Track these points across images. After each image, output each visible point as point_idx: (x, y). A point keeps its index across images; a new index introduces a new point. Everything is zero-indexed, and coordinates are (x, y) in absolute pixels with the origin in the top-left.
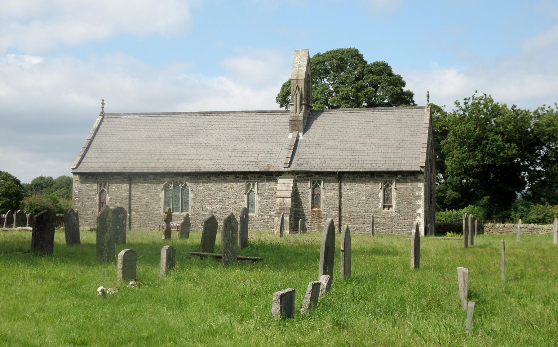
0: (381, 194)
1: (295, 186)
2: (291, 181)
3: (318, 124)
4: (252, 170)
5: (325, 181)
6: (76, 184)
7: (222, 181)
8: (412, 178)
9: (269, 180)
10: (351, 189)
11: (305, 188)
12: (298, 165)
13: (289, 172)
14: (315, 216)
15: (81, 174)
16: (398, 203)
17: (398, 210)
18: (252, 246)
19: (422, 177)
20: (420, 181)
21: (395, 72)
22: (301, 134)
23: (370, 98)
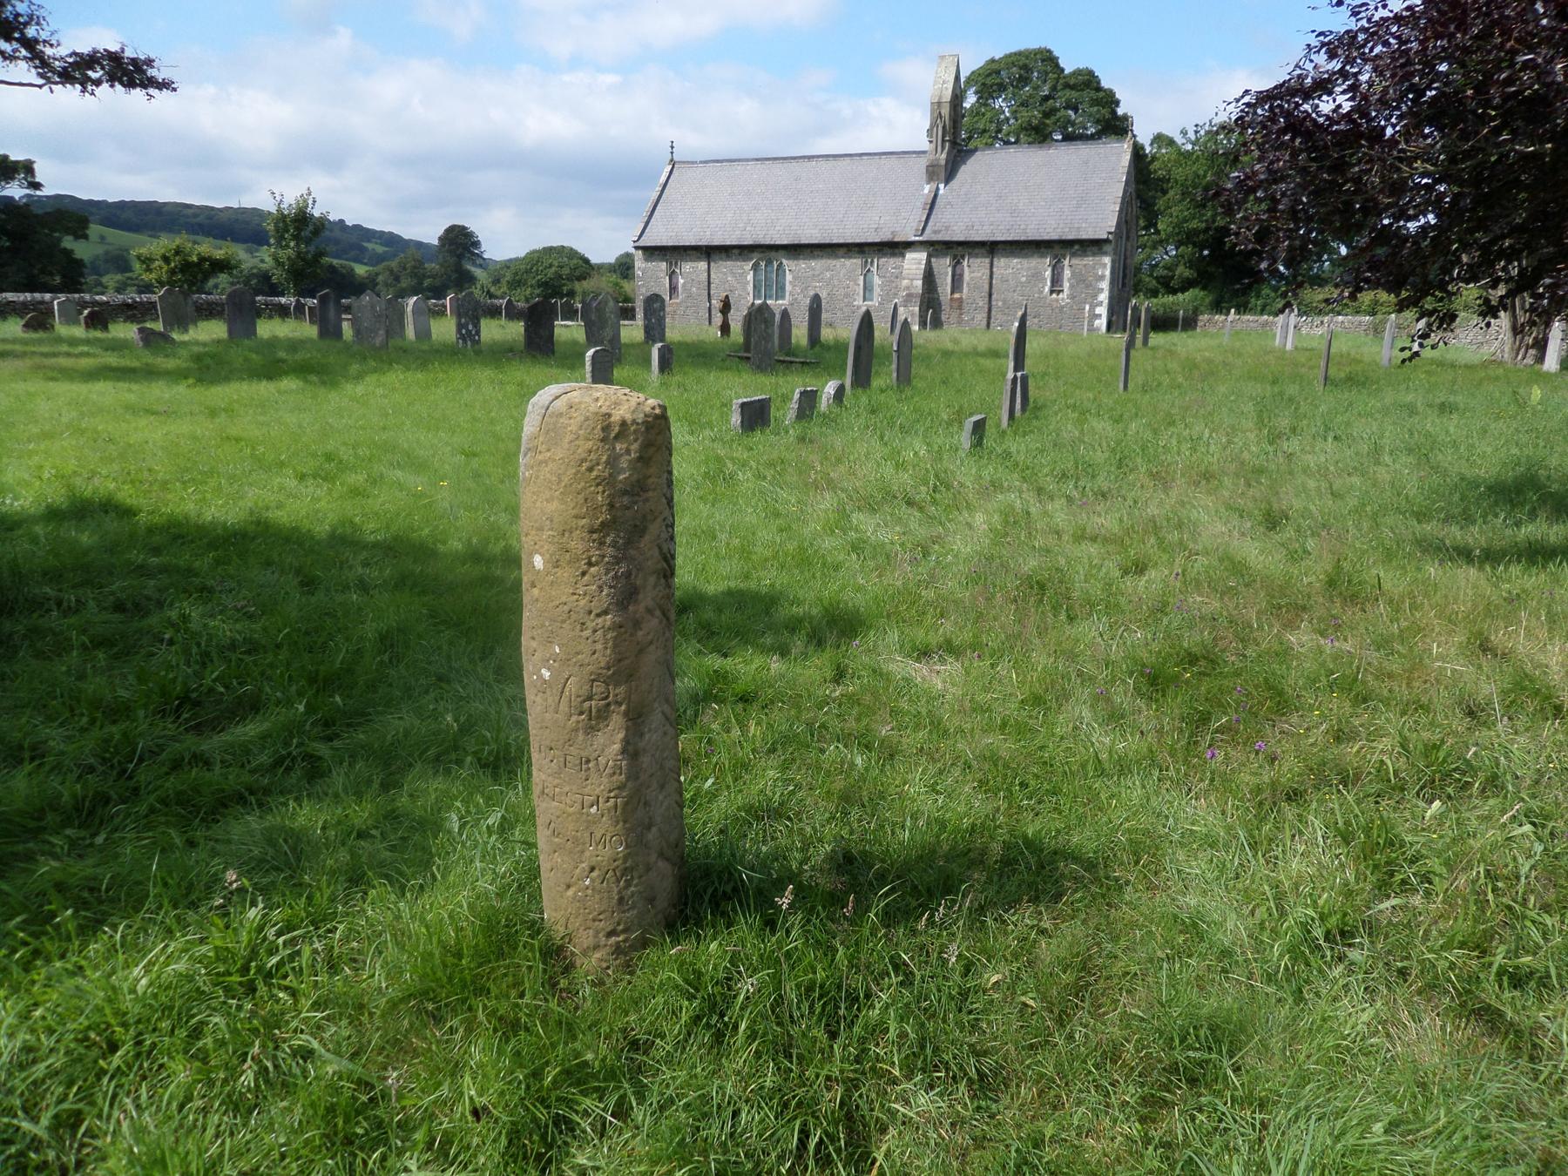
0: (1048, 273)
1: (929, 262)
2: (923, 256)
3: (966, 171)
4: (870, 240)
5: (971, 256)
6: (640, 263)
7: (830, 256)
8: (1095, 249)
9: (893, 255)
10: (1008, 267)
11: (943, 266)
12: (935, 232)
13: (921, 243)
14: (955, 305)
15: (645, 249)
16: (1072, 286)
17: (1072, 297)
18: (822, 346)
19: (1108, 248)
20: (1105, 254)
21: (1105, 84)
22: (942, 186)
23: (1065, 128)
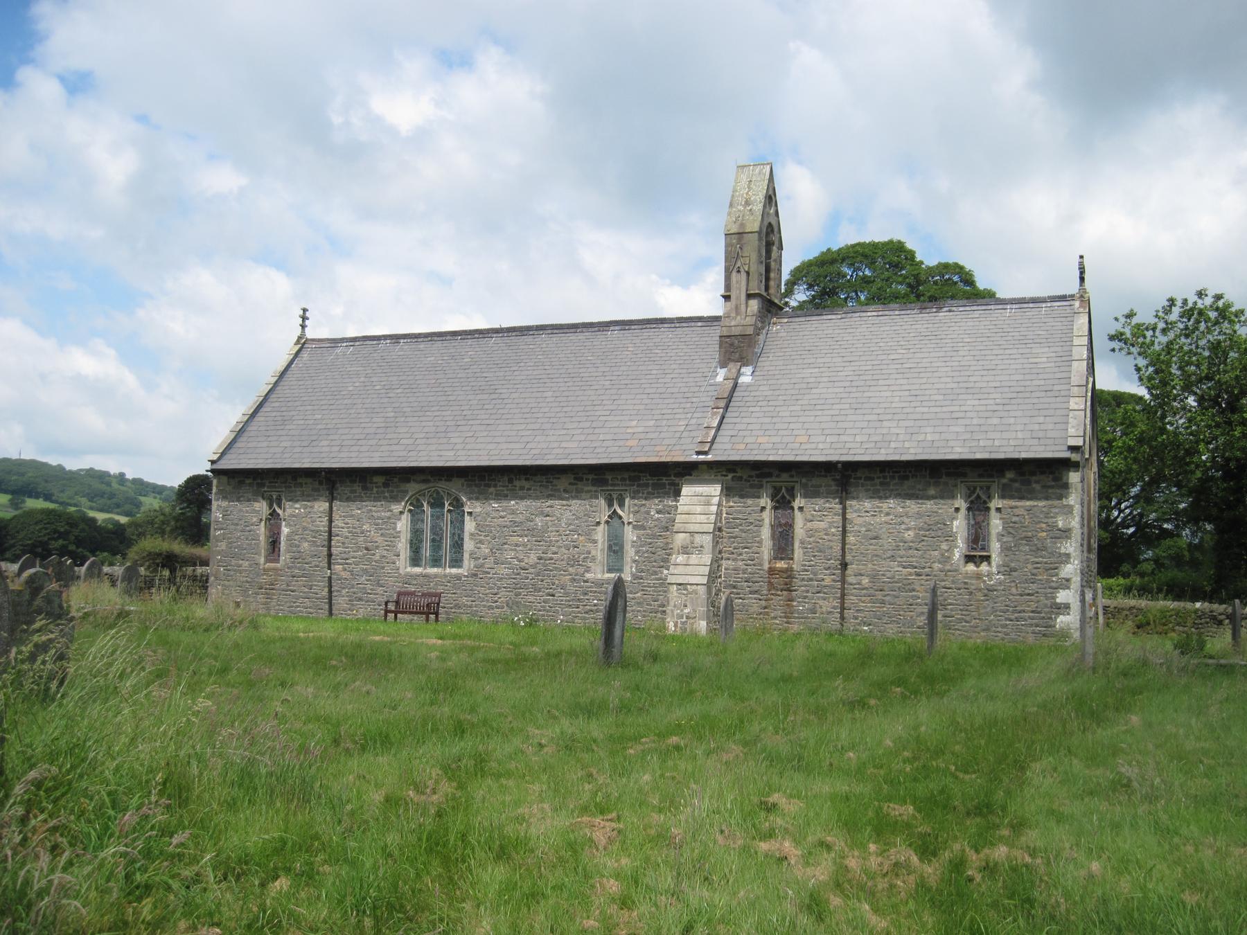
16: (1006, 549)
